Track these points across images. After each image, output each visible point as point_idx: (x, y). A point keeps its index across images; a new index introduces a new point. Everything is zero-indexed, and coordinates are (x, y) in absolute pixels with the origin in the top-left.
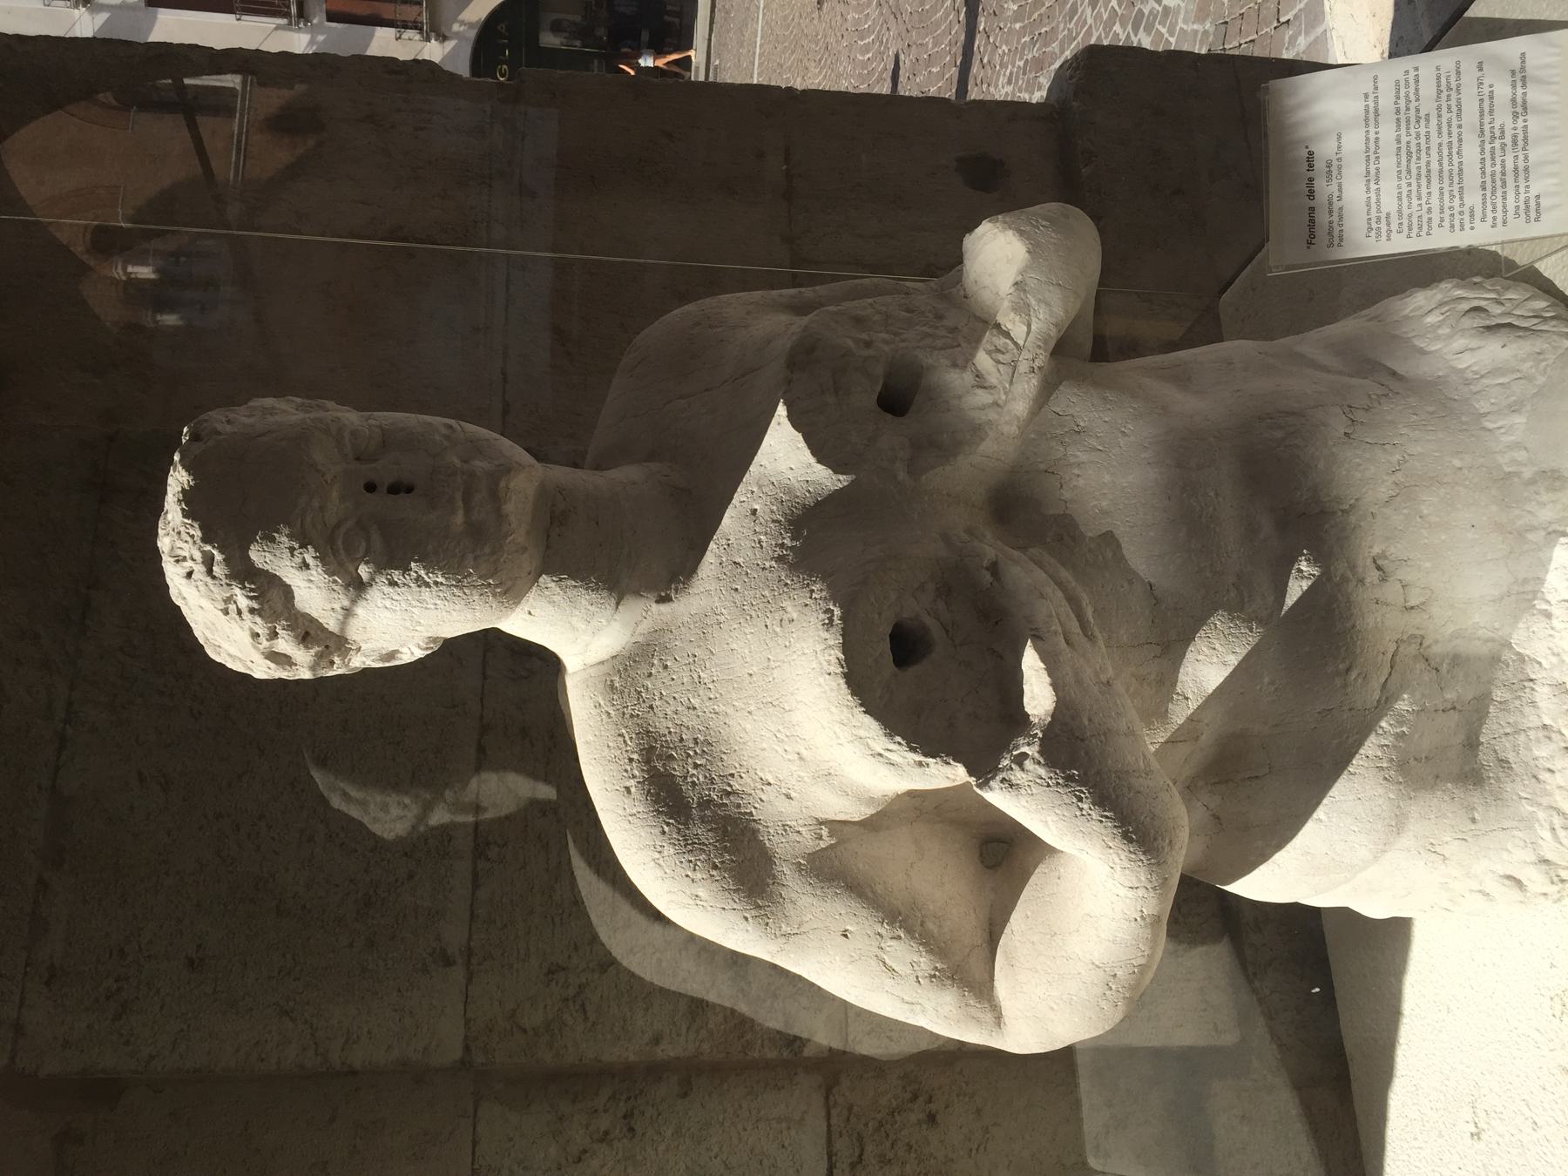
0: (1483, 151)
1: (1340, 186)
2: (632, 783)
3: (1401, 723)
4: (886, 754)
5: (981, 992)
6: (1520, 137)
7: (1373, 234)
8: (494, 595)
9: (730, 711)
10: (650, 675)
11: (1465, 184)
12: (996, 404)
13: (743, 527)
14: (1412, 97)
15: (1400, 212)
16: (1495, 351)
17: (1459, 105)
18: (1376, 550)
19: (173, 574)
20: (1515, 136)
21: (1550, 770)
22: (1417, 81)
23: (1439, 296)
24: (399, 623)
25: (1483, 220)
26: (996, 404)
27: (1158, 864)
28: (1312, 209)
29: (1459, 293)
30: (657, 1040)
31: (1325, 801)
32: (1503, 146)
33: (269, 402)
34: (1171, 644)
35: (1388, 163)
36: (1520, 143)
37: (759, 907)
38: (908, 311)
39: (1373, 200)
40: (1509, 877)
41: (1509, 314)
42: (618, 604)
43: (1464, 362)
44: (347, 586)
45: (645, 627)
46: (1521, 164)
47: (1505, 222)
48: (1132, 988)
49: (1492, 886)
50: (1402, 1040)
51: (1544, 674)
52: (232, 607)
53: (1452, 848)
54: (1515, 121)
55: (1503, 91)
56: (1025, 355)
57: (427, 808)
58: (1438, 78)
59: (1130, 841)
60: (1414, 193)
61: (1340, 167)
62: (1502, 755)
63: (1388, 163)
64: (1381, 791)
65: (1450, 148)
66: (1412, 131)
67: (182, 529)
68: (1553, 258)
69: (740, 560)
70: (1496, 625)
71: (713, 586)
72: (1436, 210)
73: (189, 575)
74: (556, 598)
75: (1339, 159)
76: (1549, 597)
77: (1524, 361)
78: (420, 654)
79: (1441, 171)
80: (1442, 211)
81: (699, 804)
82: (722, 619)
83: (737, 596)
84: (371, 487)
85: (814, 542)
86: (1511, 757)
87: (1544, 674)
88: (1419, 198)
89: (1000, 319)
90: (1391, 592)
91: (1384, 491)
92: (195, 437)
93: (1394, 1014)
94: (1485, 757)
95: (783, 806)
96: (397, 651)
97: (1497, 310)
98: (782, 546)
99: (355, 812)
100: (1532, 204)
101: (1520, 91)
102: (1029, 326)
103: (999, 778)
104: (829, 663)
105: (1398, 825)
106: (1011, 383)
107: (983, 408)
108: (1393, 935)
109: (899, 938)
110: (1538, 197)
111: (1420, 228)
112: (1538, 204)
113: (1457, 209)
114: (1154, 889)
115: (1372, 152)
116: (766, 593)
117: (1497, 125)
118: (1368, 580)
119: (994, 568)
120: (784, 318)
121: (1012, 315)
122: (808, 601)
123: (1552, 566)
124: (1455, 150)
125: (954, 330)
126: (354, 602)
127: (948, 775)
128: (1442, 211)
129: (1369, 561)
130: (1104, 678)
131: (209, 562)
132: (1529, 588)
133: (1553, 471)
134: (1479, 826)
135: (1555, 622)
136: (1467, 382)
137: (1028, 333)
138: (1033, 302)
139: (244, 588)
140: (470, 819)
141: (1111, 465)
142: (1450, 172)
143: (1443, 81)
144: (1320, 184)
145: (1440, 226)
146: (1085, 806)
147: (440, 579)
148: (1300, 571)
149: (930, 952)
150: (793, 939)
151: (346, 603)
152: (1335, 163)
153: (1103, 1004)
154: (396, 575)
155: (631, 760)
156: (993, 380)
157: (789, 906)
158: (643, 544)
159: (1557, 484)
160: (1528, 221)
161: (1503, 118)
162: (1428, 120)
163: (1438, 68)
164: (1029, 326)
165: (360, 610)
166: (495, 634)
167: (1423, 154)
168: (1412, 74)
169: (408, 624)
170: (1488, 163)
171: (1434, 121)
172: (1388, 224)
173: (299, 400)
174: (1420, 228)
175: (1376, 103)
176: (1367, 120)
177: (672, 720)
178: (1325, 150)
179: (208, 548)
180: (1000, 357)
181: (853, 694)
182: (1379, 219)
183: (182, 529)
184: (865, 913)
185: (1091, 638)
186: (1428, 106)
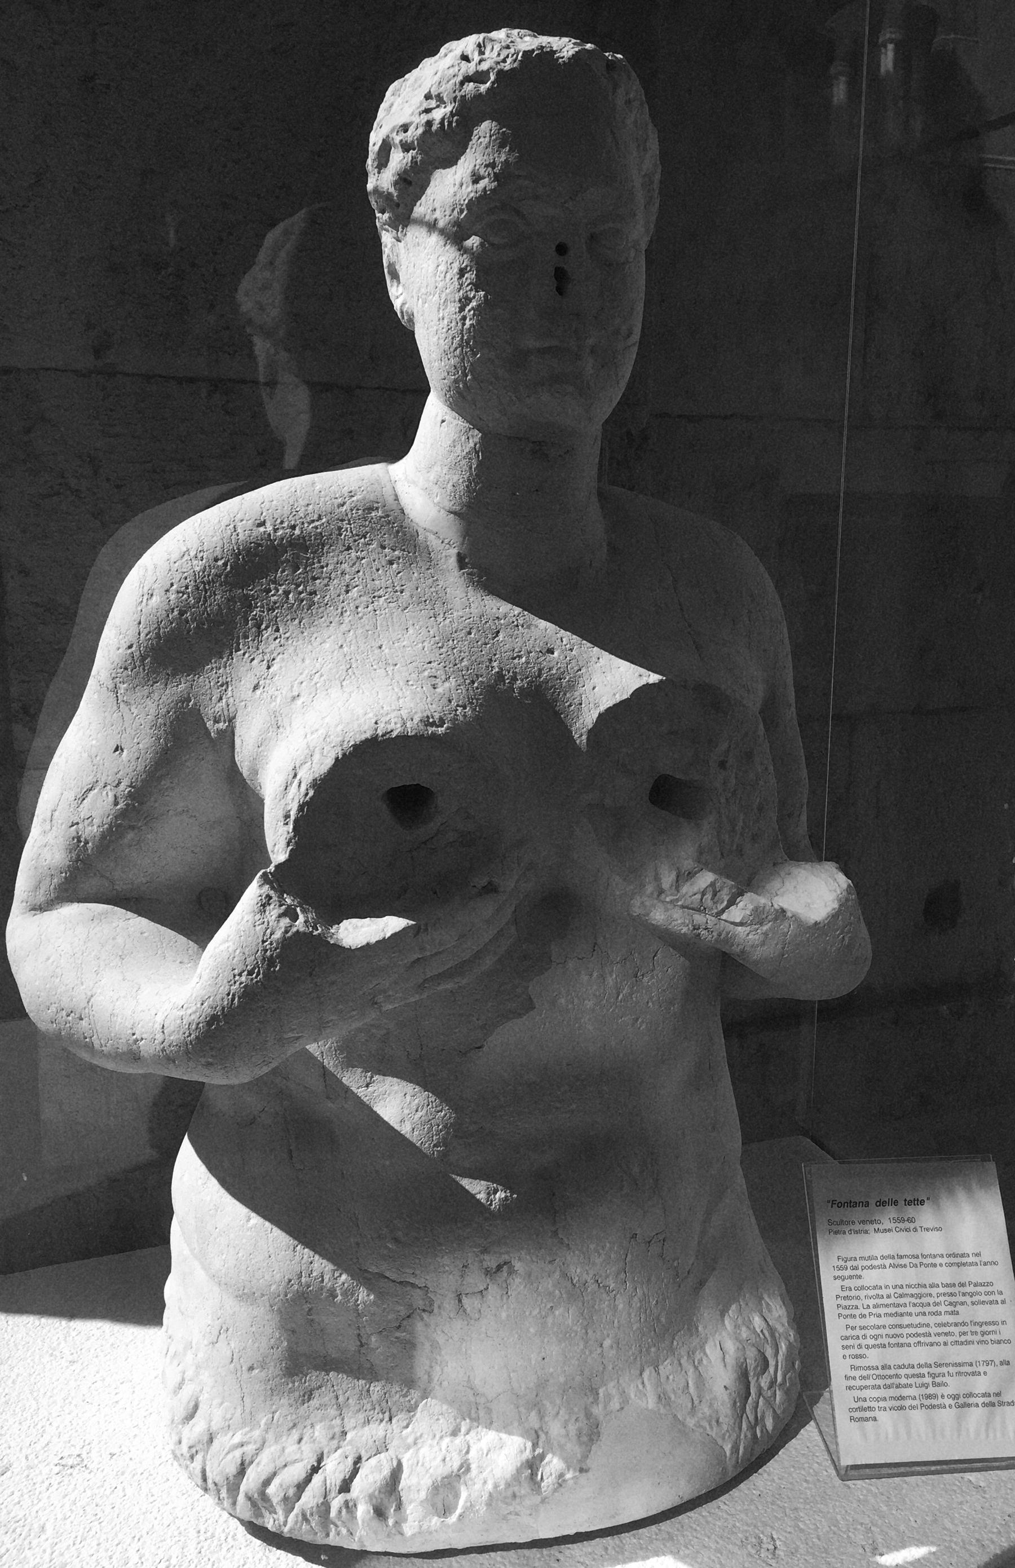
0: (920, 1366)
1: (890, 1230)
2: (269, 528)
3: (345, 1293)
4: (296, 781)
5: (66, 890)
6: (934, 1402)
7: (841, 1263)
8: (456, 381)
9: (344, 627)
10: (383, 547)
11: (888, 1350)
12: (661, 892)
13: (540, 640)
14: (976, 1298)
15: (862, 1288)
16: (720, 1377)
17: (968, 1343)
18: (518, 1265)
19: (469, 43)
20: (935, 1396)
21: (300, 1440)
22: (991, 1302)
23: (781, 1329)
24: (425, 280)
25: (853, 1367)
26: (661, 892)
27: (187, 1052)
28: (867, 1204)
29: (783, 1347)
30: (24, 572)
31: (267, 1224)
32: (926, 1386)
33: (654, 145)
34: (416, 1070)
35: (910, 1276)
36: (928, 1402)
37: (143, 658)
38: (760, 809)
39: (875, 1263)
40: (196, 1407)
41: (760, 1394)
42: (455, 513)
43: (712, 1351)
44: (457, 223)
45: (434, 542)
46: (908, 1403)
47: (850, 1388)
48: (70, 1036)
49: (188, 1391)
50: (43, 1320)
51: (397, 1431)
52: (433, 103)
53: (224, 1350)
54: (950, 1396)
55: (981, 1385)
56: (711, 920)
57: (268, 334)
58: (994, 1323)
59: (209, 1024)
60: (880, 1301)
61: (907, 1230)
62: (316, 1393)
63: (910, 1276)
64: (278, 1277)
65: (924, 1335)
66: (942, 1299)
67: (512, 51)
68: (819, 1438)
69: (501, 637)
70: (445, 1384)
71: (475, 610)
72: (863, 1322)
73: (465, 58)
74: (458, 448)
75: (915, 1230)
76: (473, 1433)
77: (711, 1406)
78: (397, 304)
79: (901, 1326)
80: (862, 1328)
81: (247, 596)
82: (440, 619)
83: (462, 634)
84: (562, 249)
85: (517, 710)
86: (314, 1403)
87: (397, 1431)
88: (875, 1307)
89: (748, 896)
90: (475, 1280)
91: (576, 1271)
92: (611, 65)
93: (71, 1313)
94: (314, 1377)
95: (247, 682)
96: (399, 282)
97: (764, 1382)
98: (514, 679)
99: (262, 256)
100: (868, 1414)
101: (980, 1400)
102: (741, 924)
103: (272, 893)
104: (388, 722)
105: (246, 1296)
106: (683, 907)
107: (657, 878)
108: (144, 1306)
109: (116, 804)
110: (875, 1419)
111: (846, 1308)
112: (867, 1419)
113: (864, 1342)
114: (163, 1050)
115: (921, 1260)
116: (465, 663)
117: (947, 1379)
118: (486, 1257)
119: (491, 889)
120: (760, 690)
121: (751, 907)
122: (454, 703)
123: (504, 1436)
124: (922, 1339)
125: (740, 852)
126: (442, 232)
127: (278, 843)
128: (862, 1328)
129: (506, 1257)
130: (380, 998)
131: (479, 77)
132: (482, 1413)
133: (599, 1434)
134: (246, 1375)
135: (447, 1440)
136: (690, 1354)
137: (732, 923)
138: (765, 928)
139: (452, 114)
140: (262, 379)
141: (602, 1007)
142: (901, 1336)
143: (991, 1328)
144: (891, 1212)
145: (847, 1327)
146: (243, 979)
147: (468, 323)
148: (495, 1192)
149: (103, 836)
150: (112, 695)
151: (441, 224)
152: (912, 1226)
153: (53, 1008)
154: (470, 276)
155: (293, 527)
156: (685, 889)
157: (146, 690)
158: (509, 537)
159: (585, 1439)
160: (851, 1410)
161: (953, 1385)
162: (952, 1313)
163: (1003, 1323)
164: (741, 924)
165: (435, 239)
166: (428, 391)
168: (999, 1298)
169: (423, 290)
170: (910, 1371)
171: (951, 1319)
172: (851, 1277)
173: (657, 177)
174: (846, 1308)
175: (971, 1264)
176: (955, 1256)
177: (335, 569)
178: (926, 1216)
179: (492, 77)
180: (708, 896)
181: (355, 746)
182: (856, 1268)
183: (512, 51)
184: (140, 768)
185: (421, 987)
186: (966, 1313)
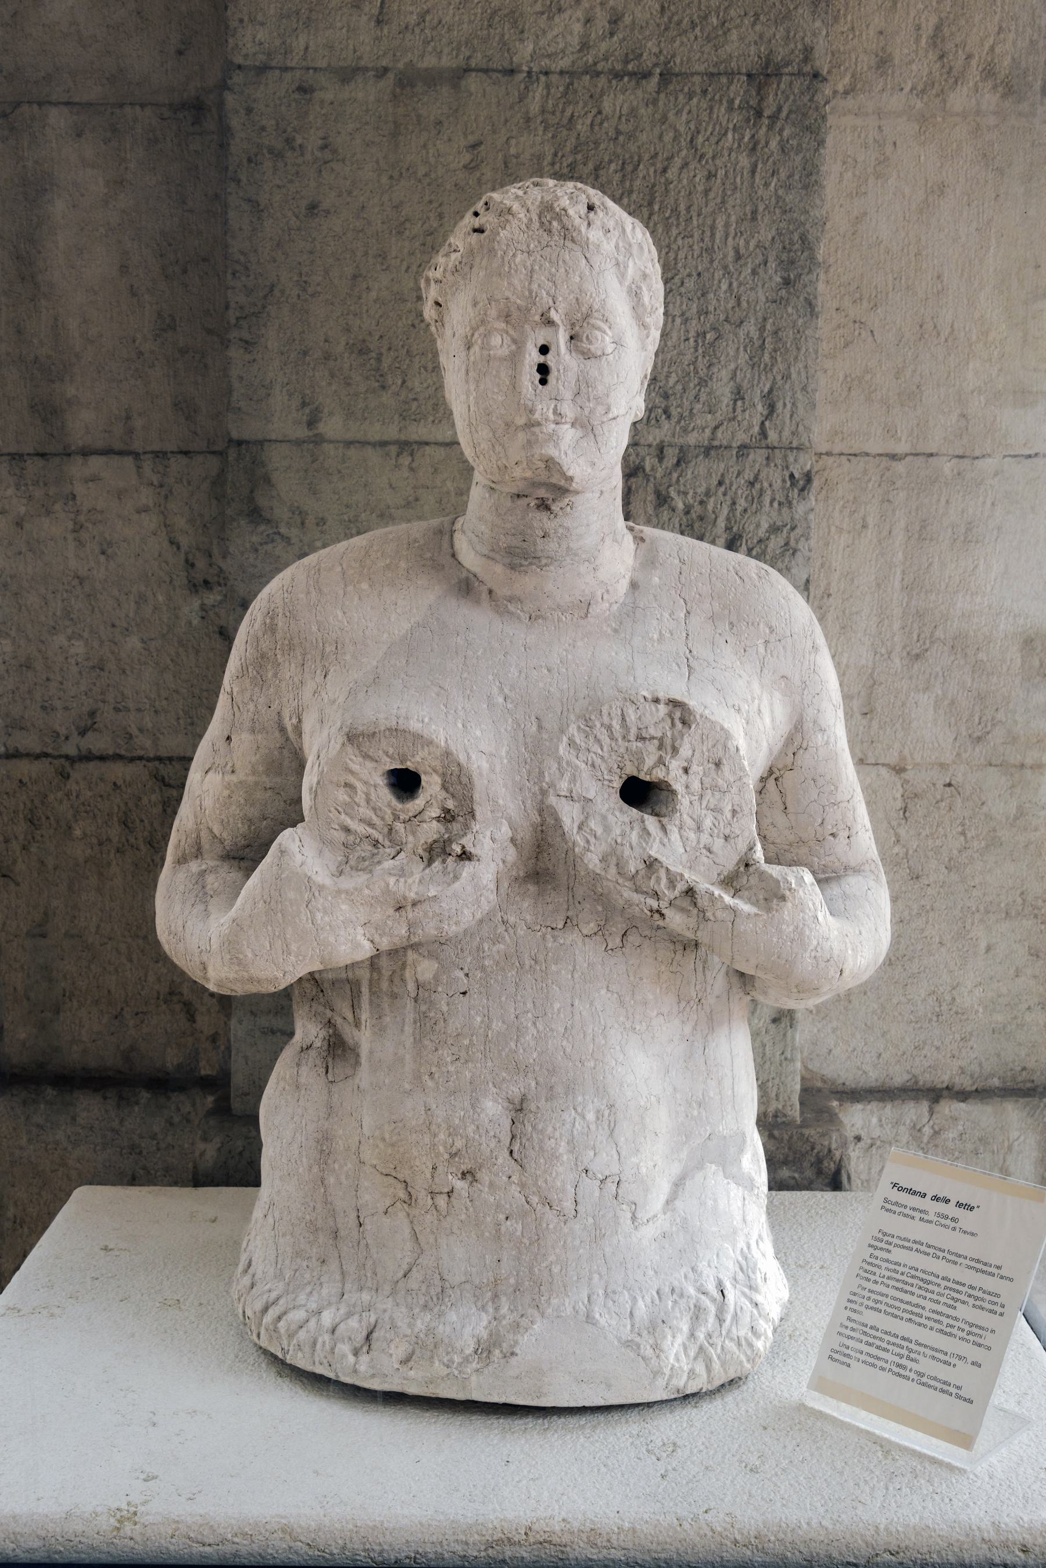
6: (902, 1372)
7: (880, 1236)
14: (978, 1303)
17: (950, 1335)
25: (849, 1319)
32: (901, 1356)
58: (980, 1328)
60: (894, 1275)
65: (917, 1315)
110: (849, 1366)
111: (866, 1271)
117: (920, 1358)
124: (913, 1317)
128: (870, 1291)
163: (993, 1331)
167: (923, 1293)
170: (893, 1340)
174: (866, 1271)
